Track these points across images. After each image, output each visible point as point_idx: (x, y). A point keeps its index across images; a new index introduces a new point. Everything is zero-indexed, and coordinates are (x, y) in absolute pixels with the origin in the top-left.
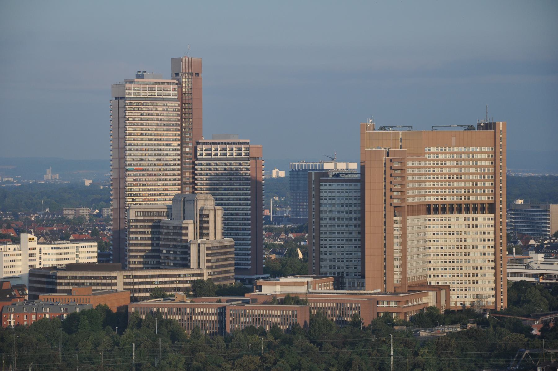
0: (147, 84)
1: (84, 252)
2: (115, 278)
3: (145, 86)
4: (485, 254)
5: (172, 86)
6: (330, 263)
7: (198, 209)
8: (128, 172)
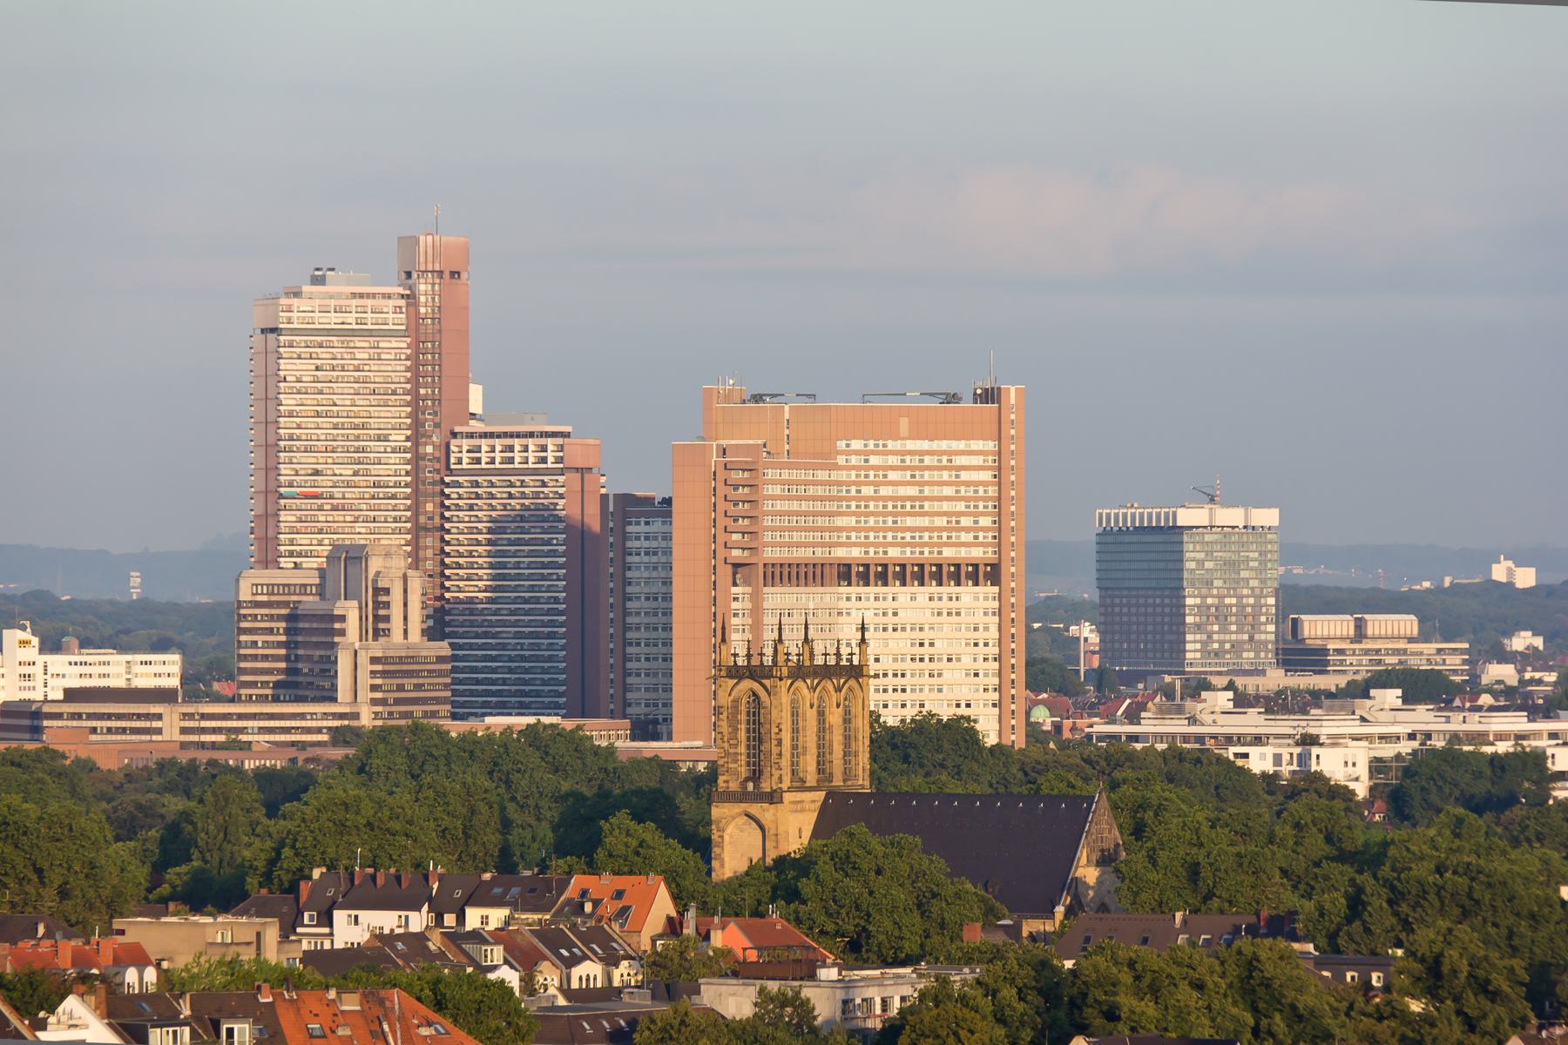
0: (331, 297)
1: (147, 675)
2: (159, 717)
3: (327, 302)
4: (976, 675)
5: (391, 303)
6: (647, 696)
7: (371, 576)
8: (282, 502)
